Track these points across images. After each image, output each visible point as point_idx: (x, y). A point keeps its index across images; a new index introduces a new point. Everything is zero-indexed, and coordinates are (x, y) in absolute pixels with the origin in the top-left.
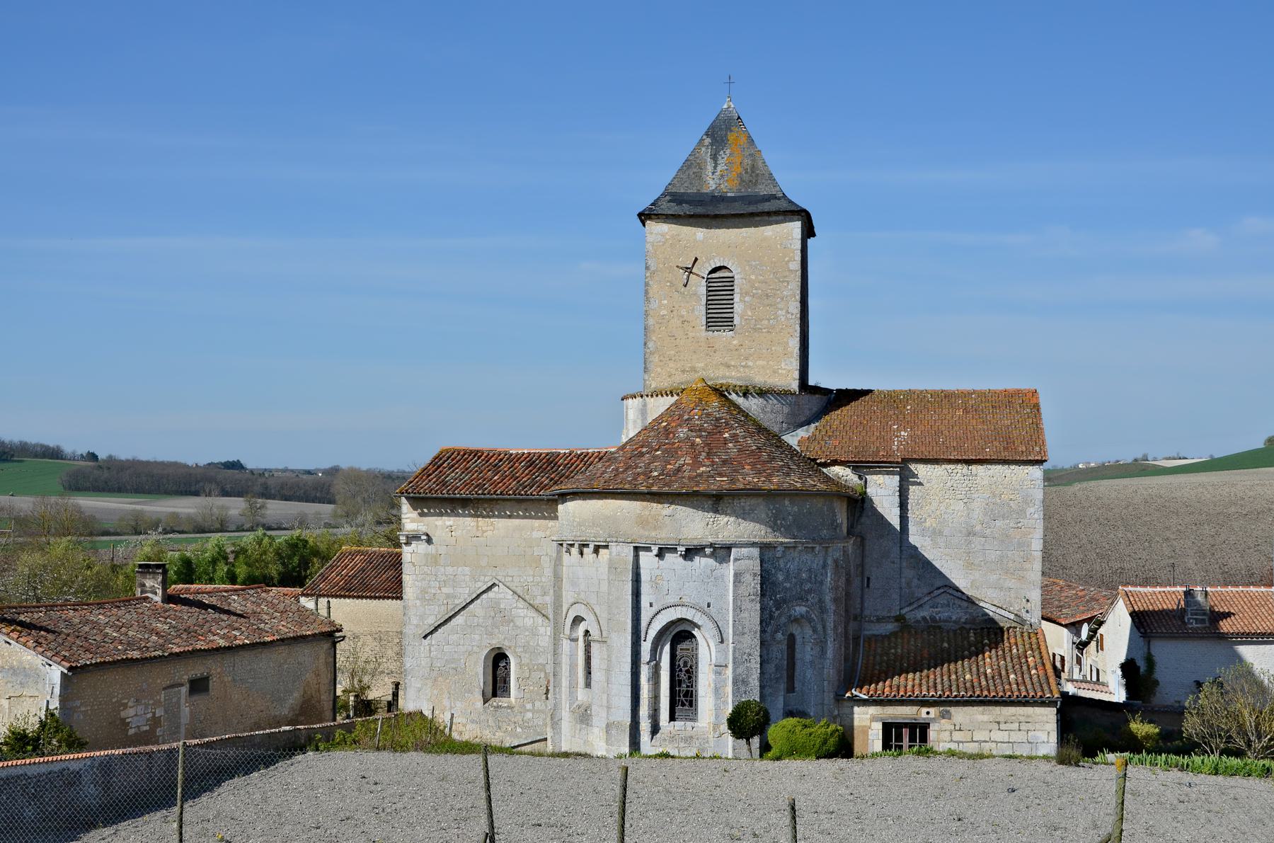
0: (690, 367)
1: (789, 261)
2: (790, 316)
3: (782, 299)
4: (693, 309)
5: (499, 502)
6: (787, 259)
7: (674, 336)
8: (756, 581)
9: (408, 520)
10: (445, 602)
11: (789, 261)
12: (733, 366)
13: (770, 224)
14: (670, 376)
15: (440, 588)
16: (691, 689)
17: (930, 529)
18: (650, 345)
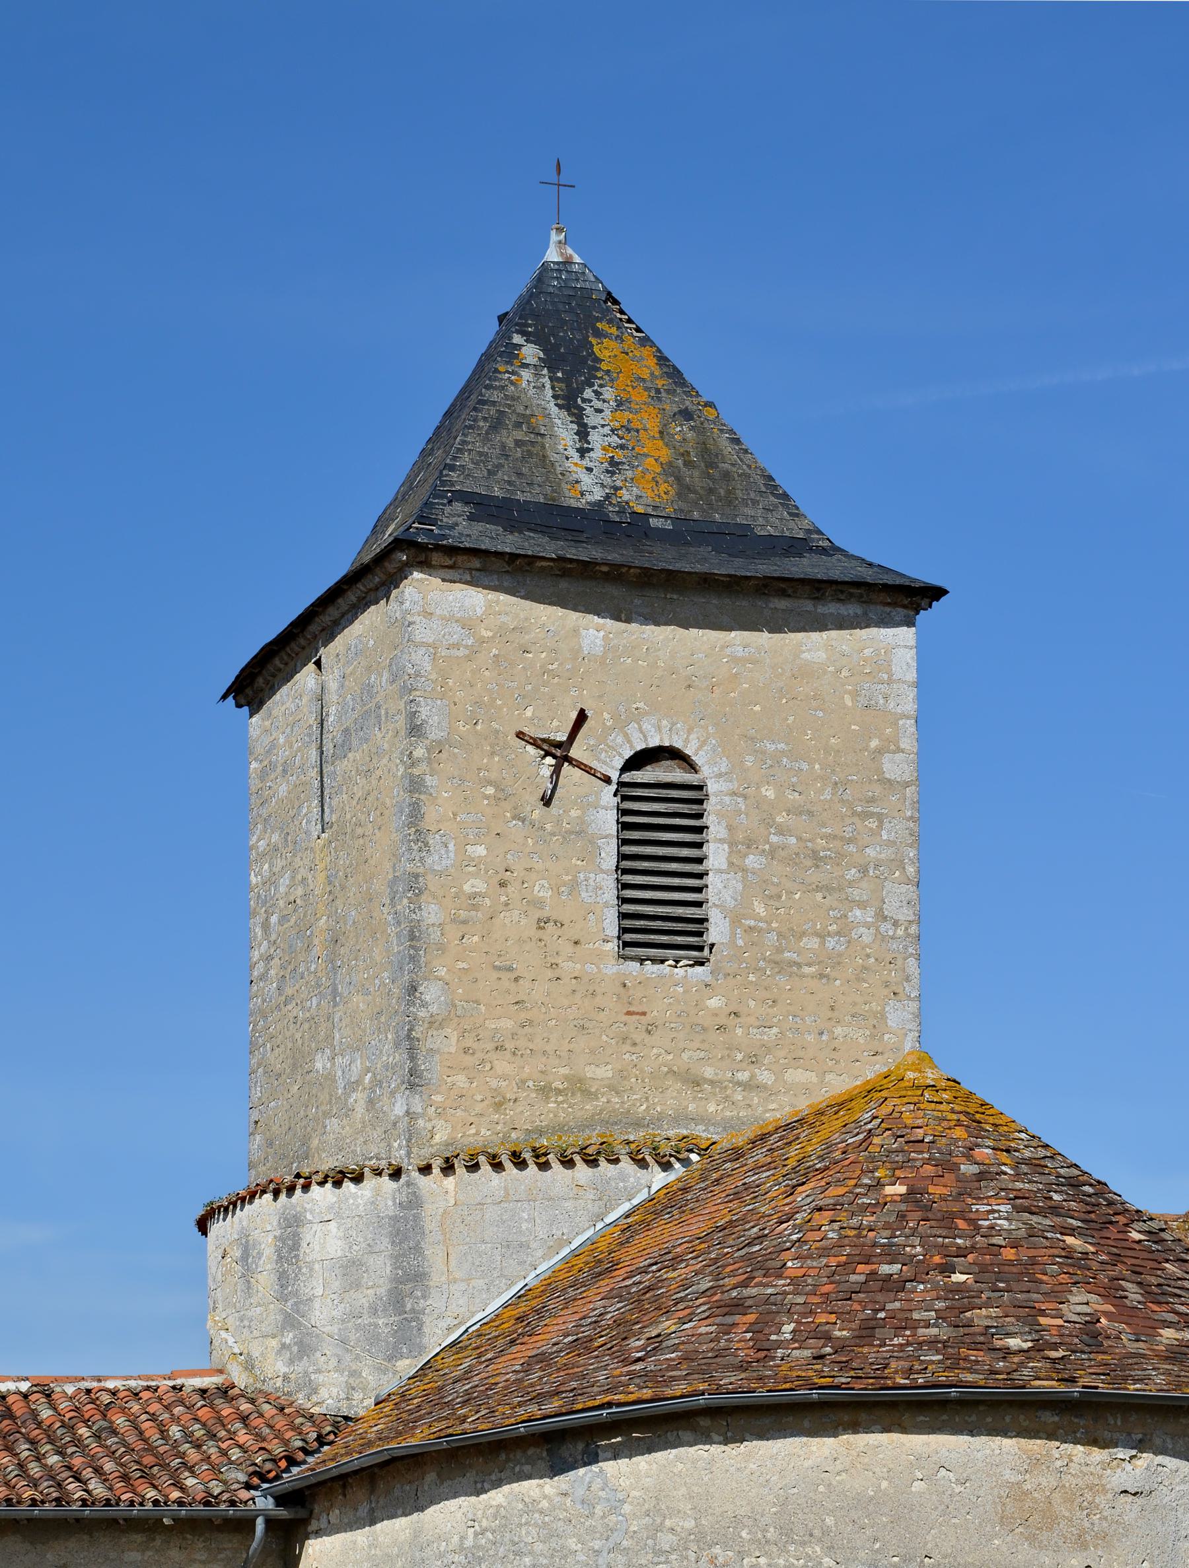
0: (566, 1078)
1: (880, 751)
6: (874, 743)
11: (880, 751)
12: (712, 1082)
13: (820, 625)
18: (430, 992)
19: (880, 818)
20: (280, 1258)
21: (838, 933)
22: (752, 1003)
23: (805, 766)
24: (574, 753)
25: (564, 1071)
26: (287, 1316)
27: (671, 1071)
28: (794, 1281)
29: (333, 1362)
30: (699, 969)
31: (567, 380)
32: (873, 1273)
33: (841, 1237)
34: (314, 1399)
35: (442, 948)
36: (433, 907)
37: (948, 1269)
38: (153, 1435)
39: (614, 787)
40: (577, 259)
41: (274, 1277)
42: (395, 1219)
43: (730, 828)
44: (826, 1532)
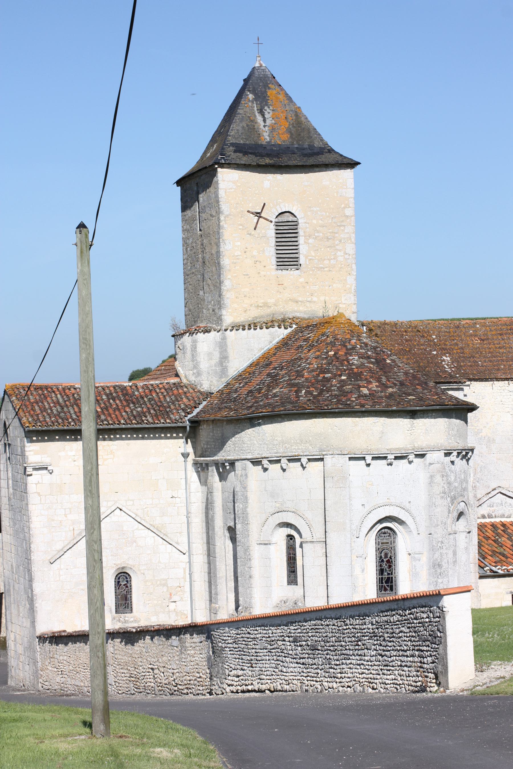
0: (263, 303)
1: (344, 208)
2: (347, 256)
3: (340, 241)
4: (264, 249)
5: (117, 432)
6: (343, 206)
7: (247, 275)
8: (444, 482)
9: (32, 453)
10: (71, 528)
11: (344, 208)
12: (301, 301)
14: (245, 311)
15: (66, 515)
16: (391, 576)
17: (486, 438)
19: (344, 226)
20: (192, 350)
21: (334, 259)
22: (311, 279)
23: (324, 214)
24: (262, 215)
25: (262, 301)
26: (194, 366)
27: (290, 299)
28: (307, 379)
29: (206, 378)
30: (297, 271)
31: (260, 104)
32: (324, 377)
33: (318, 367)
34: (202, 387)
35: (230, 271)
36: (227, 260)
37: (340, 376)
38: (162, 399)
39: (273, 223)
40: (264, 65)
41: (191, 356)
42: (220, 342)
43: (304, 232)
44: (310, 441)
